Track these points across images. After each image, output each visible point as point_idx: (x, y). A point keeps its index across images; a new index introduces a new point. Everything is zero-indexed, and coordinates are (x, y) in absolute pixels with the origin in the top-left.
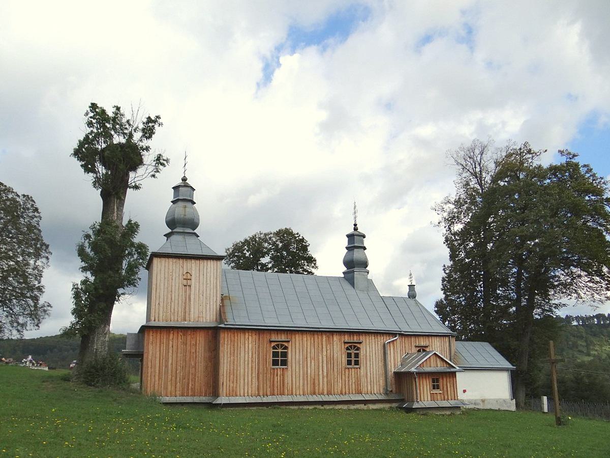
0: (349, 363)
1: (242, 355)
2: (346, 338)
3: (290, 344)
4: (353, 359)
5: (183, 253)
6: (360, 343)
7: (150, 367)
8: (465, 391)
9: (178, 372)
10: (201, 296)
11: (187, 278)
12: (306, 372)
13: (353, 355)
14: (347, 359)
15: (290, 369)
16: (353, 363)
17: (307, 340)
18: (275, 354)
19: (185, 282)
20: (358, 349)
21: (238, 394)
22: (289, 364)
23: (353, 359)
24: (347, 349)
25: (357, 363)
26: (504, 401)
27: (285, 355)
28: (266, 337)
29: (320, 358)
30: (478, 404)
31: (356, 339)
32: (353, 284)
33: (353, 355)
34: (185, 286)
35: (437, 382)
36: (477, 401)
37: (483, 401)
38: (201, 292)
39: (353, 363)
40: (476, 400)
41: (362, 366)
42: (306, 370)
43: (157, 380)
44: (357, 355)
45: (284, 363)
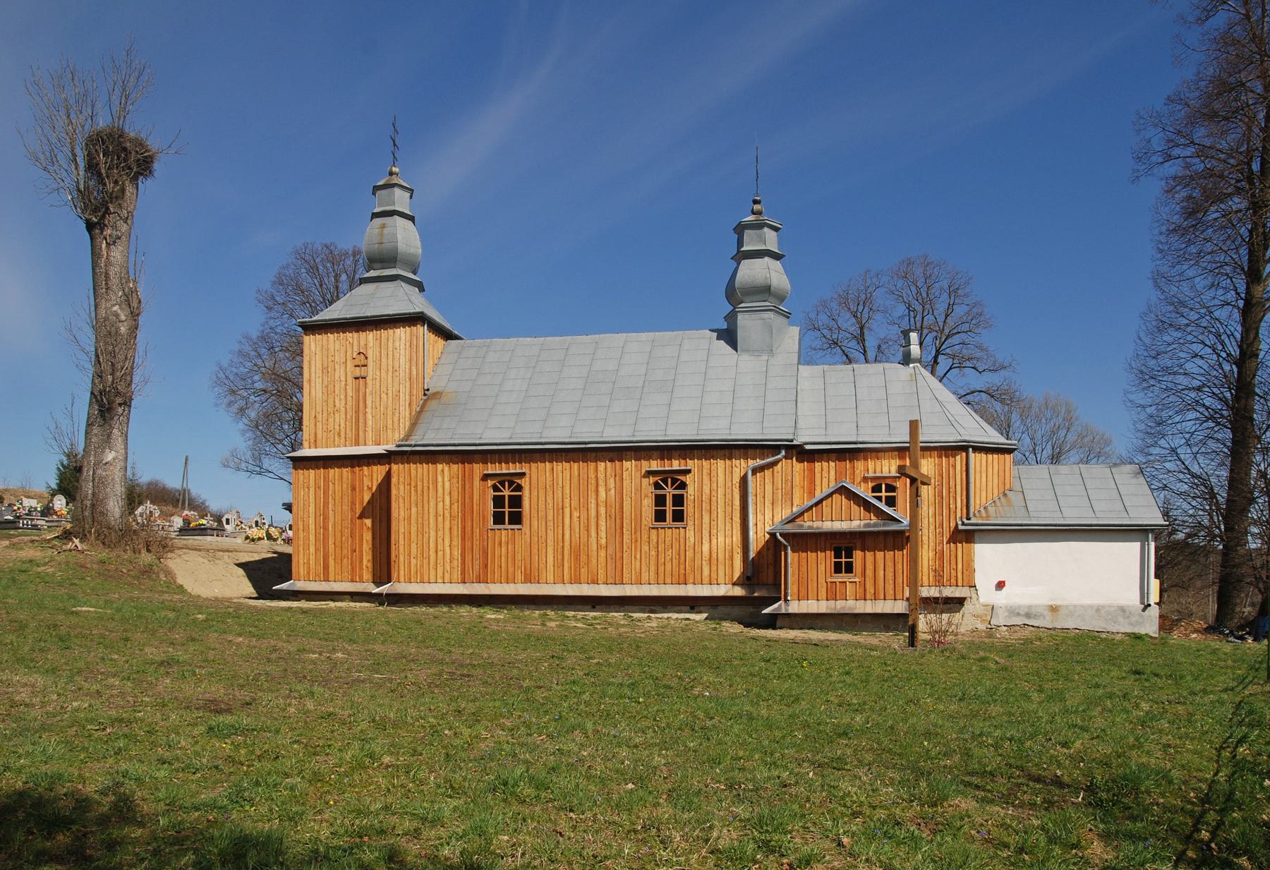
0: (660, 516)
1: (432, 504)
2: (655, 465)
3: (527, 479)
4: (669, 508)
5: (348, 316)
6: (689, 471)
7: (301, 527)
8: (1000, 585)
9: (344, 538)
10: (384, 396)
11: (361, 361)
12: (560, 536)
13: (669, 501)
14: (685, 508)
15: (528, 532)
16: (669, 516)
17: (563, 470)
18: (498, 501)
19: (358, 372)
20: (683, 486)
21: (426, 579)
22: (526, 520)
23: (669, 508)
24: (657, 486)
25: (679, 516)
26: (1123, 609)
27: (516, 502)
28: (478, 469)
29: (593, 506)
30: (1036, 617)
31: (676, 465)
32: (733, 344)
33: (669, 501)
34: (355, 378)
35: (849, 555)
36: (1033, 611)
37: (1054, 609)
38: (384, 389)
39: (669, 516)
40: (1030, 607)
41: (690, 523)
42: (561, 532)
43: (448, 561)
44: (678, 500)
45: (516, 519)
